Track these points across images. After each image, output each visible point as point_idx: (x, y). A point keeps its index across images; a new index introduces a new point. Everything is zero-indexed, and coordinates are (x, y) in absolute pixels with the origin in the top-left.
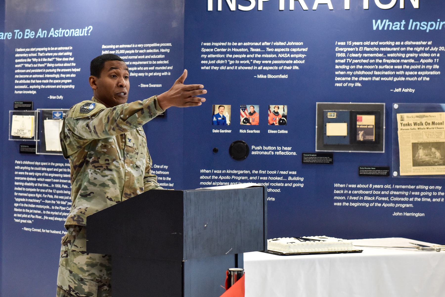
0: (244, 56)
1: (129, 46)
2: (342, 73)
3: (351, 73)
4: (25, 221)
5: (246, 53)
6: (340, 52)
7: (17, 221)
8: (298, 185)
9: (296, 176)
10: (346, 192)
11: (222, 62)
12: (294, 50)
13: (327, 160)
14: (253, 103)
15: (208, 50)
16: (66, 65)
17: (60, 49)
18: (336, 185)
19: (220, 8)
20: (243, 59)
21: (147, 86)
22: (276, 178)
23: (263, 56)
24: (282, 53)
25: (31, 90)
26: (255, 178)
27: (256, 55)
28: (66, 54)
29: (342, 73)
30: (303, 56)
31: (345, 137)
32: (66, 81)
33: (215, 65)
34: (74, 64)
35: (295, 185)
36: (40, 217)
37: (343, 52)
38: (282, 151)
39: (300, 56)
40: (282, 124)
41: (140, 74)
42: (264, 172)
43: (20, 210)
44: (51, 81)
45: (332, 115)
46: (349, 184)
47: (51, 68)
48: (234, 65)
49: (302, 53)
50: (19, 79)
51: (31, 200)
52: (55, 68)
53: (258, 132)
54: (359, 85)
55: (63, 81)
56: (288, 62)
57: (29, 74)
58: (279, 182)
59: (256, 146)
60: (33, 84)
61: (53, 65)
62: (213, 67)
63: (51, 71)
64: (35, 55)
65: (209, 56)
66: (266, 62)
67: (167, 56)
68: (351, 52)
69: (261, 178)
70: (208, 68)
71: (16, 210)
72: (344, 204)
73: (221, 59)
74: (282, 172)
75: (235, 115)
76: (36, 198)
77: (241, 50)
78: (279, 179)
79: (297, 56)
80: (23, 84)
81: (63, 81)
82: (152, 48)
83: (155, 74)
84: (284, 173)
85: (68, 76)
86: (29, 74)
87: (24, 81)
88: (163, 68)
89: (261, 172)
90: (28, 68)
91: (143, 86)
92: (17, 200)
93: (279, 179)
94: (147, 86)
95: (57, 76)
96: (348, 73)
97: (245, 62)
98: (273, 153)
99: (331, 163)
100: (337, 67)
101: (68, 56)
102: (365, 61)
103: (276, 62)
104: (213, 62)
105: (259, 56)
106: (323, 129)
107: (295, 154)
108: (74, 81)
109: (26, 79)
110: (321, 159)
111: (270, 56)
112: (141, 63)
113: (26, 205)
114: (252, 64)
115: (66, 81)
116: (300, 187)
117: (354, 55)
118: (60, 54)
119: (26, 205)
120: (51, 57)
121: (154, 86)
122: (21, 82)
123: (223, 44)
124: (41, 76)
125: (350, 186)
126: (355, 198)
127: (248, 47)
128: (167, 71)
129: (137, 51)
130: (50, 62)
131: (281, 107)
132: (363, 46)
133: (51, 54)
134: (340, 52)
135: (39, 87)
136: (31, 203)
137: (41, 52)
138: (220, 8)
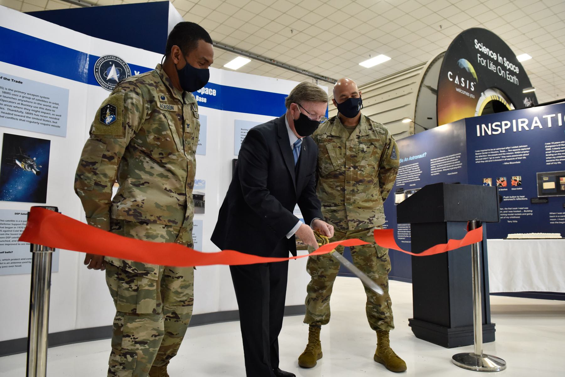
0: (497, 155)
1: (442, 158)
2: (550, 158)
3: (555, 158)
4: (402, 238)
5: (498, 153)
6: (548, 148)
7: (399, 238)
8: (530, 214)
9: (528, 210)
10: (556, 216)
11: (486, 158)
12: (523, 149)
13: (545, 201)
14: (503, 176)
15: (478, 154)
16: (416, 171)
17: (413, 164)
18: (551, 213)
19: (483, 134)
20: (496, 156)
21: (451, 174)
22: (517, 211)
23: (507, 154)
24: (516, 151)
25: (403, 183)
26: (506, 212)
27: (503, 154)
28: (416, 166)
29: (550, 158)
30: (528, 152)
31: (554, 189)
32: (416, 178)
33: (483, 160)
34: (419, 170)
35: (528, 214)
36: (408, 236)
37: (549, 148)
38: (520, 198)
39: (526, 152)
40: (519, 185)
41: (448, 169)
42: (511, 209)
43: (400, 234)
44: (410, 178)
45: (545, 179)
46: (558, 212)
47: (410, 173)
48: (492, 159)
49: (527, 150)
50: (398, 180)
51: (404, 229)
52: (412, 173)
53: (507, 190)
54: (560, 163)
55: (415, 178)
56: (520, 155)
57: (402, 177)
58: (519, 213)
59: (506, 196)
60: (403, 181)
61: (411, 172)
62: (481, 162)
63: (410, 174)
64: (404, 169)
65: (479, 157)
66: (509, 156)
67: (459, 159)
68: (554, 147)
69: (510, 212)
70: (479, 162)
71: (398, 234)
72: (556, 222)
73: (485, 157)
74: (520, 208)
75: (494, 183)
76: (406, 228)
77: (495, 152)
78: (519, 211)
79: (525, 152)
80: (399, 182)
81: (415, 178)
82: (452, 157)
83: (454, 168)
84: (522, 208)
85: (417, 175)
86: (402, 177)
87: (400, 180)
88: (458, 165)
89: (509, 209)
90: (401, 175)
91: (449, 174)
92: (399, 230)
93: (519, 211)
94: (451, 174)
95: (413, 176)
96: (553, 157)
97: (497, 157)
98: (515, 199)
99: (547, 202)
100: (547, 155)
101: (417, 167)
102: (562, 151)
103: (514, 156)
104: (482, 159)
105: (505, 154)
106: (541, 186)
107: (527, 199)
108: (420, 177)
109: (400, 179)
110: (541, 201)
111: (510, 153)
112: (447, 164)
113: (402, 232)
114: (501, 158)
115: (416, 178)
116: (531, 215)
117: (556, 149)
118: (414, 167)
119: (402, 232)
120: (410, 169)
121: (454, 173)
122: (399, 181)
123: (486, 150)
124: (406, 177)
125: (559, 213)
126: (562, 219)
127: (499, 151)
128: (459, 166)
129: (446, 160)
130: (410, 171)
131: (518, 177)
132: (561, 144)
133: (410, 167)
134: (548, 148)
135: (406, 182)
136: (404, 231)
137: (406, 167)
138: (483, 134)
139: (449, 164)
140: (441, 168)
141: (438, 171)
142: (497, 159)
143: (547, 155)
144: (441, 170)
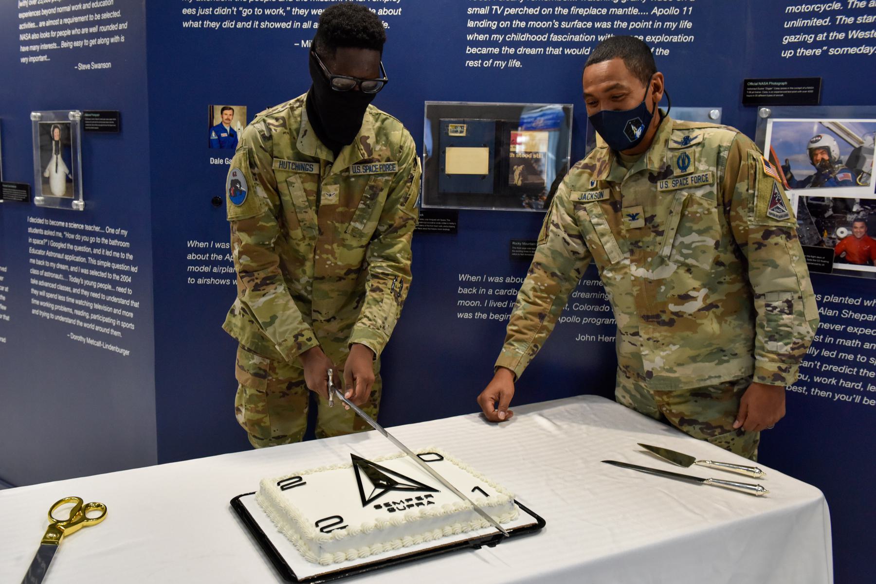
13: (446, 225)
21: (88, 67)
41: (78, 44)
62: (207, 23)
88: (113, 27)
94: (88, 67)
97: (274, 12)
99: (454, 231)
114: (288, 17)
128: (118, 33)
139: (82, 19)
140: (53, 34)
141: (45, 47)
142: (271, 18)
143: (471, 24)
144: (53, 46)
